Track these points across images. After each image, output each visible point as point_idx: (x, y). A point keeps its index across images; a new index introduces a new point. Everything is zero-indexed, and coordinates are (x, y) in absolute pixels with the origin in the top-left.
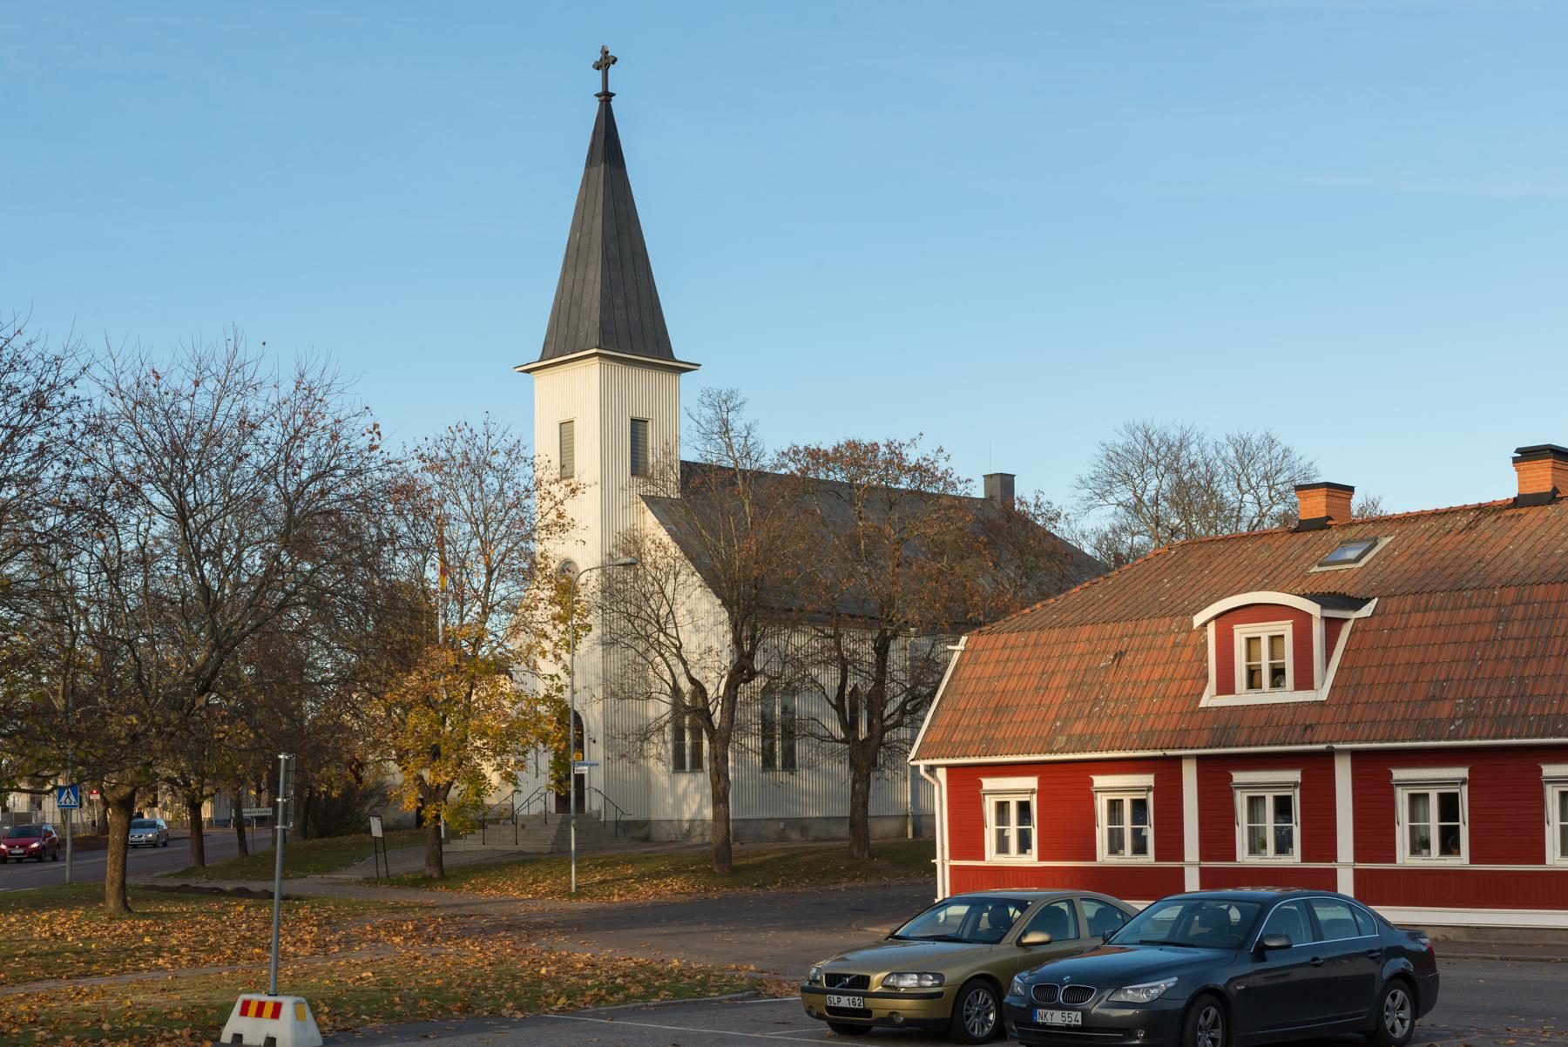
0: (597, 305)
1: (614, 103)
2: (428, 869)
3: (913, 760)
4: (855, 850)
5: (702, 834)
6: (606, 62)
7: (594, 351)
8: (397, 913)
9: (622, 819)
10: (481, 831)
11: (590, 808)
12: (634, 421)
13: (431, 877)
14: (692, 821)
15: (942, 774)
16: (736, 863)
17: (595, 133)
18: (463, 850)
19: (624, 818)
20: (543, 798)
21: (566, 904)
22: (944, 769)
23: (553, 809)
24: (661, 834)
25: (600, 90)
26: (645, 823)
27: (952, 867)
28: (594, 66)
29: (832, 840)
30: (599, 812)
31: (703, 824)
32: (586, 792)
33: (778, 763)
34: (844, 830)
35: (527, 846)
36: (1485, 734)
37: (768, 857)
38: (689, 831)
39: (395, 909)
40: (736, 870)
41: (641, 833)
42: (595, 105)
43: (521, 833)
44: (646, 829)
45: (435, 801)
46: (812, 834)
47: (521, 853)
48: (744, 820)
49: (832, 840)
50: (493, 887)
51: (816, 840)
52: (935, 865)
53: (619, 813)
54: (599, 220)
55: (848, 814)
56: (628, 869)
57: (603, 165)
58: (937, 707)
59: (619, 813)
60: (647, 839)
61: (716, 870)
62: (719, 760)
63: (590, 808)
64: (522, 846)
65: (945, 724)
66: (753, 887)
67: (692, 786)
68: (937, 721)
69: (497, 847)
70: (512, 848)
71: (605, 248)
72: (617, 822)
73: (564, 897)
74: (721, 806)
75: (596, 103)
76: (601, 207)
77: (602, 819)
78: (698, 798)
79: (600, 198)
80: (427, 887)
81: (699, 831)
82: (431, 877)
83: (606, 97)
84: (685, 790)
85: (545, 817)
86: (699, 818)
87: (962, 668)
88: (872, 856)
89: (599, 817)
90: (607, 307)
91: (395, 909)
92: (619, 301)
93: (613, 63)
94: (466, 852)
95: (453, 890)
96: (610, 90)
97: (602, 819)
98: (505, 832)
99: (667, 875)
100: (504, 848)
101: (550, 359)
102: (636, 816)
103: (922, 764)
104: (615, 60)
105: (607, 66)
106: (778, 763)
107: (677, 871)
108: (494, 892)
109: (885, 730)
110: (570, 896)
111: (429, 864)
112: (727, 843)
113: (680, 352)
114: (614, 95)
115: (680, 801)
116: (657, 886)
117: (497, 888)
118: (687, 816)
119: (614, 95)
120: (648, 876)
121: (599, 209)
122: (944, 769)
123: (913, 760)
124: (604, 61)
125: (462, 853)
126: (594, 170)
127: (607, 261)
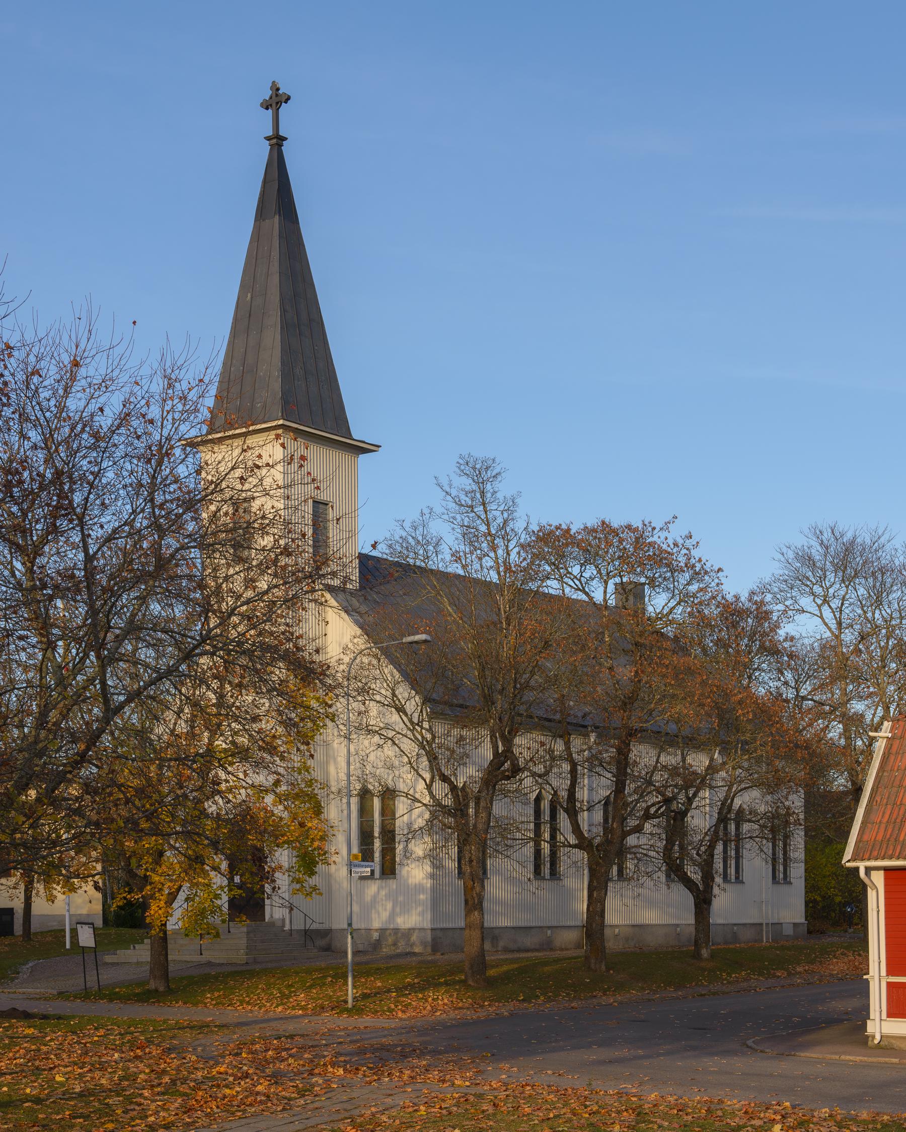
1: (286, 148)
2: (152, 982)
3: (849, 861)
5: (395, 944)
7: (281, 422)
11: (272, 917)
13: (156, 991)
14: (382, 931)
15: (878, 878)
16: (491, 972)
17: (265, 182)
18: (135, 961)
19: (315, 926)
21: (345, 1021)
22: (882, 872)
25: (270, 133)
27: (889, 985)
28: (262, 105)
29: (519, 950)
30: (283, 920)
31: (396, 934)
36: (867, 856)
37: (505, 968)
38: (378, 941)
46: (501, 944)
47: (209, 964)
48: (441, 929)
49: (519, 950)
51: (506, 950)
52: (867, 981)
54: (275, 280)
58: (869, 801)
59: (309, 921)
61: (470, 982)
62: (474, 863)
64: (207, 956)
65: (885, 820)
67: (383, 893)
70: (196, 958)
71: (284, 311)
74: (476, 913)
75: (266, 147)
76: (276, 264)
77: (287, 927)
78: (389, 906)
79: (275, 254)
80: (159, 1001)
81: (390, 940)
82: (156, 991)
83: (277, 141)
84: (375, 897)
86: (392, 926)
87: (892, 758)
89: (284, 926)
90: (287, 374)
93: (286, 102)
96: (281, 134)
97: (287, 927)
100: (188, 958)
102: (325, 926)
103: (862, 866)
104: (288, 98)
105: (279, 104)
109: (626, 834)
113: (359, 432)
114: (285, 139)
115: (369, 908)
118: (376, 925)
119: (285, 139)
121: (275, 267)
122: (882, 872)
123: (849, 861)
124: (275, 99)
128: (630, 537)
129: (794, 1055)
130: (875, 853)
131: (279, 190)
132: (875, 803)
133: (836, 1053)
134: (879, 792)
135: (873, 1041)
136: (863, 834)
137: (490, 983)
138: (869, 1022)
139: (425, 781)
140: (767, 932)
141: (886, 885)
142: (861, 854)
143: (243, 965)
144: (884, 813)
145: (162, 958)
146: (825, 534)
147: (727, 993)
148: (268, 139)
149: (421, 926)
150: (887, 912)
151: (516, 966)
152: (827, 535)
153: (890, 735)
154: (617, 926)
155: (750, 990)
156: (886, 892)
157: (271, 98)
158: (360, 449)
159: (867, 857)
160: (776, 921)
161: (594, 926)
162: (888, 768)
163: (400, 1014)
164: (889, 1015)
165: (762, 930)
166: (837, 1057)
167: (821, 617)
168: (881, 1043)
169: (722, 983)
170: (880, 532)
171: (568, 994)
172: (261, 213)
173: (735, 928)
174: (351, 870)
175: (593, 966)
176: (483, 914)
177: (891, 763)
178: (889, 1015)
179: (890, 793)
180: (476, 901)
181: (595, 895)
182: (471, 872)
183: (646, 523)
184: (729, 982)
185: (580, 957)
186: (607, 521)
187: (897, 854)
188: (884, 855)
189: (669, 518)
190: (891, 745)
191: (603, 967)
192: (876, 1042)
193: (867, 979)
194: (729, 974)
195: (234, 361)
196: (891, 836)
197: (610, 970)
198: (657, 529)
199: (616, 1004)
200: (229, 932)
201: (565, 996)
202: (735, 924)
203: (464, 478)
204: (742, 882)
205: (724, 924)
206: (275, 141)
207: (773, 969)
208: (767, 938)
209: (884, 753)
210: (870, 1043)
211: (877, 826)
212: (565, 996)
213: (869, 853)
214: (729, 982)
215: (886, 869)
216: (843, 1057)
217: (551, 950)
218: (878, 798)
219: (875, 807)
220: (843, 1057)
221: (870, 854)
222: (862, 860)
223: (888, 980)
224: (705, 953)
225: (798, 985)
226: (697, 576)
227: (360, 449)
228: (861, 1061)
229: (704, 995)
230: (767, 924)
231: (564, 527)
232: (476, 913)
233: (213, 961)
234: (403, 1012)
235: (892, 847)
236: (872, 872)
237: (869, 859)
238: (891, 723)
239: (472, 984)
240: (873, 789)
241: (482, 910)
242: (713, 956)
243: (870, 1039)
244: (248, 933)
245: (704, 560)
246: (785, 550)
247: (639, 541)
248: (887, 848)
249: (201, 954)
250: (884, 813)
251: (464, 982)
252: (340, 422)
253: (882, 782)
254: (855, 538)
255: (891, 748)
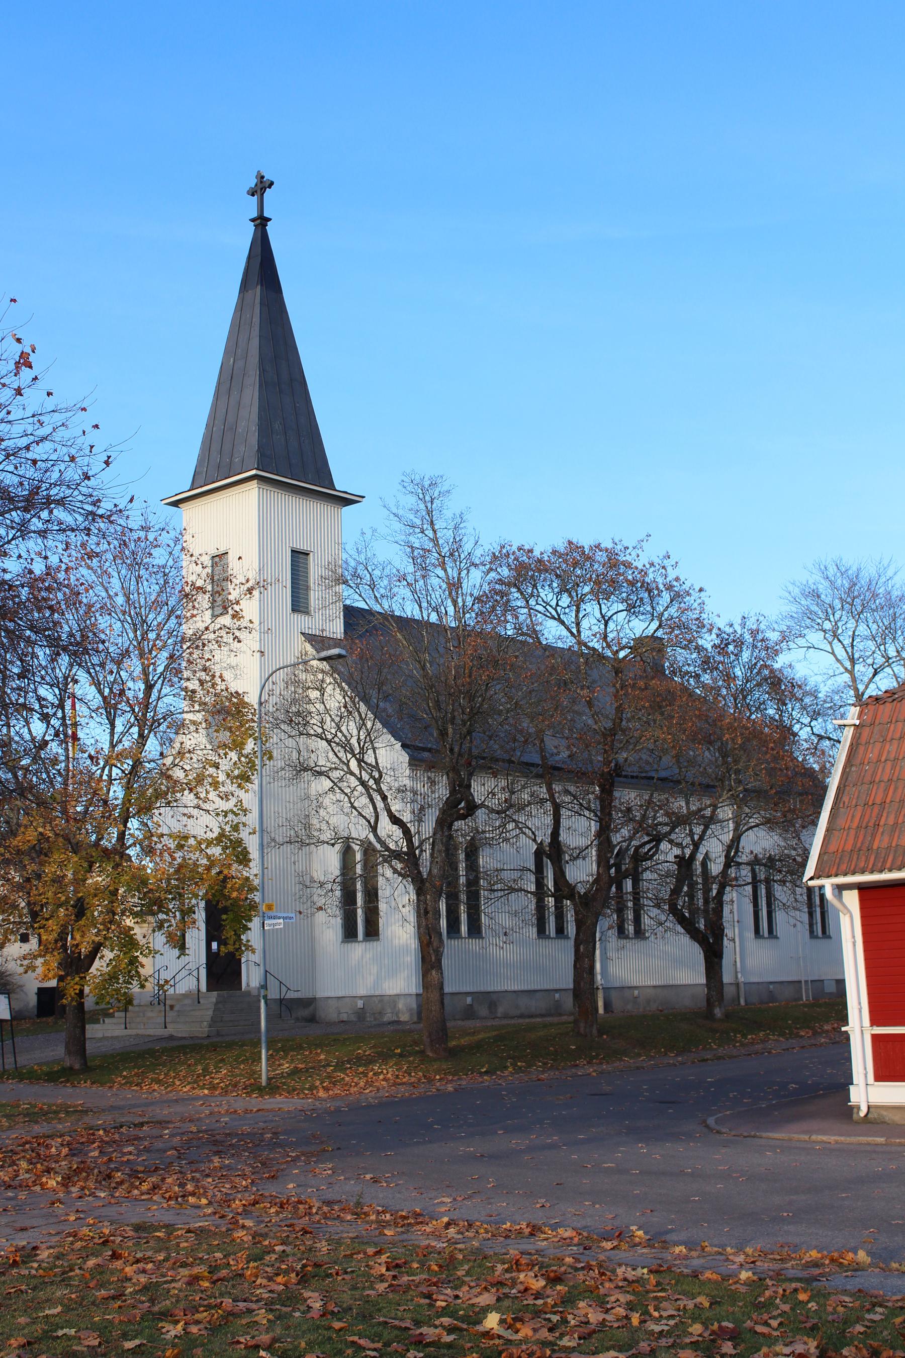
0: (254, 428)
1: (270, 227)
2: (67, 1059)
3: (811, 879)
4: (582, 1025)
6: (261, 187)
7: (254, 472)
8: (36, 1122)
9: (287, 997)
10: (122, 1014)
11: (248, 985)
12: (295, 553)
15: (852, 899)
18: (101, 1036)
19: (291, 995)
20: (195, 973)
21: (255, 1102)
23: (203, 987)
24: (330, 1013)
25: (255, 214)
26: (309, 1002)
27: (875, 1038)
32: (243, 967)
33: (464, 928)
34: (568, 1002)
35: (179, 1029)
37: (481, 1036)
39: (33, 1116)
40: (453, 1053)
41: (305, 1013)
42: (250, 230)
43: (171, 1015)
44: (312, 1008)
45: (77, 973)
47: (171, 1038)
50: (153, 1080)
51: (506, 1016)
53: (284, 989)
54: (255, 342)
55: (571, 986)
56: (318, 1054)
57: (259, 287)
59: (284, 989)
60: (312, 1019)
63: (248, 985)
64: (171, 1030)
65: (855, 825)
66: (481, 1074)
67: (368, 956)
68: (841, 822)
69: (140, 1032)
70: (160, 1032)
71: (263, 370)
72: (281, 1000)
73: (253, 1091)
74: (434, 972)
75: (251, 228)
78: (374, 970)
79: (256, 320)
80: (67, 1081)
82: (71, 1068)
83: (261, 222)
85: (197, 996)
87: (861, 749)
88: (601, 1033)
91: (33, 1116)
92: (277, 426)
94: (104, 1038)
95: (102, 1085)
96: (266, 215)
98: (150, 1014)
99: (370, 1061)
100: (151, 1032)
101: (201, 487)
102: (309, 995)
103: (828, 884)
104: (272, 184)
105: (263, 190)
106: (464, 928)
107: (384, 1056)
108: (156, 1087)
110: (261, 1090)
111: (69, 1052)
112: (444, 1021)
113: (342, 482)
114: (269, 220)
116: (365, 1075)
117: (158, 1081)
119: (269, 220)
120: (349, 1062)
123: (811, 879)
124: (260, 186)
125: (101, 1039)
126: (249, 294)
127: (264, 384)
128: (601, 557)
129: (754, 1137)
130: (843, 867)
131: (261, 264)
132: (841, 805)
133: (804, 1132)
134: (846, 792)
135: (858, 1113)
136: (828, 843)
137: (453, 1053)
138: (851, 1087)
139: (369, 822)
140: (807, 990)
141: (862, 908)
142: (827, 869)
143: (203, 1038)
144: (853, 816)
145: (78, 1031)
146: (831, 570)
147: (735, 1057)
148: (253, 220)
149: (406, 992)
150: (865, 943)
151: (494, 1033)
152: (832, 570)
153: (857, 722)
154: (636, 988)
155: (763, 1053)
156: (863, 917)
157: (256, 185)
158: (345, 501)
159: (833, 872)
160: (816, 978)
161: (582, 984)
162: (857, 761)
163: (322, 1094)
164: (879, 1077)
165: (801, 988)
166: (806, 1137)
167: (833, 653)
168: (870, 1116)
169: (734, 1046)
170: (885, 562)
171: (545, 1064)
172: (245, 285)
173: (771, 987)
174: (263, 923)
175: (582, 1030)
176: (442, 973)
177: (860, 756)
178: (879, 1077)
179: (859, 792)
180: (433, 958)
181: (582, 950)
182: (427, 925)
183: (616, 541)
184: (742, 1045)
185: (570, 1023)
186: (575, 541)
187: (870, 866)
188: (855, 869)
189: (643, 536)
190: (860, 734)
191: (595, 1031)
192: (862, 1114)
193: (846, 1032)
194: (744, 1036)
195: (216, 422)
196: (862, 843)
197: (603, 1034)
198: (631, 549)
199: (594, 1074)
200: (199, 1002)
201: (540, 1067)
202: (771, 983)
203: (409, 496)
204: (776, 937)
205: (758, 983)
206: (259, 221)
207: (797, 1028)
208: (807, 996)
209: (852, 744)
210: (855, 1116)
211: (845, 833)
212: (540, 1067)
213: (835, 867)
214: (742, 1045)
215: (862, 888)
216: (814, 1137)
217: (560, 1015)
218: (845, 799)
219: (842, 810)
220: (814, 1137)
221: (838, 868)
222: (829, 876)
223: (873, 1032)
224: (718, 1012)
225: (821, 1045)
226: (677, 597)
227: (345, 501)
228: (837, 1142)
229: (707, 1060)
230: (806, 982)
231: (527, 547)
232: (434, 972)
233: (175, 1034)
234: (326, 1089)
235: (863, 858)
236: (845, 893)
237: (836, 875)
238: (858, 708)
239: (431, 1054)
240: (838, 788)
241: (441, 968)
242: (728, 1016)
243: (855, 1110)
244: (217, 1003)
245: (683, 580)
246: (791, 588)
247: (613, 562)
248: (858, 859)
249: (166, 1027)
250: (853, 816)
251: (422, 1052)
252: (323, 474)
253: (850, 779)
254: (859, 570)
255: (859, 738)
